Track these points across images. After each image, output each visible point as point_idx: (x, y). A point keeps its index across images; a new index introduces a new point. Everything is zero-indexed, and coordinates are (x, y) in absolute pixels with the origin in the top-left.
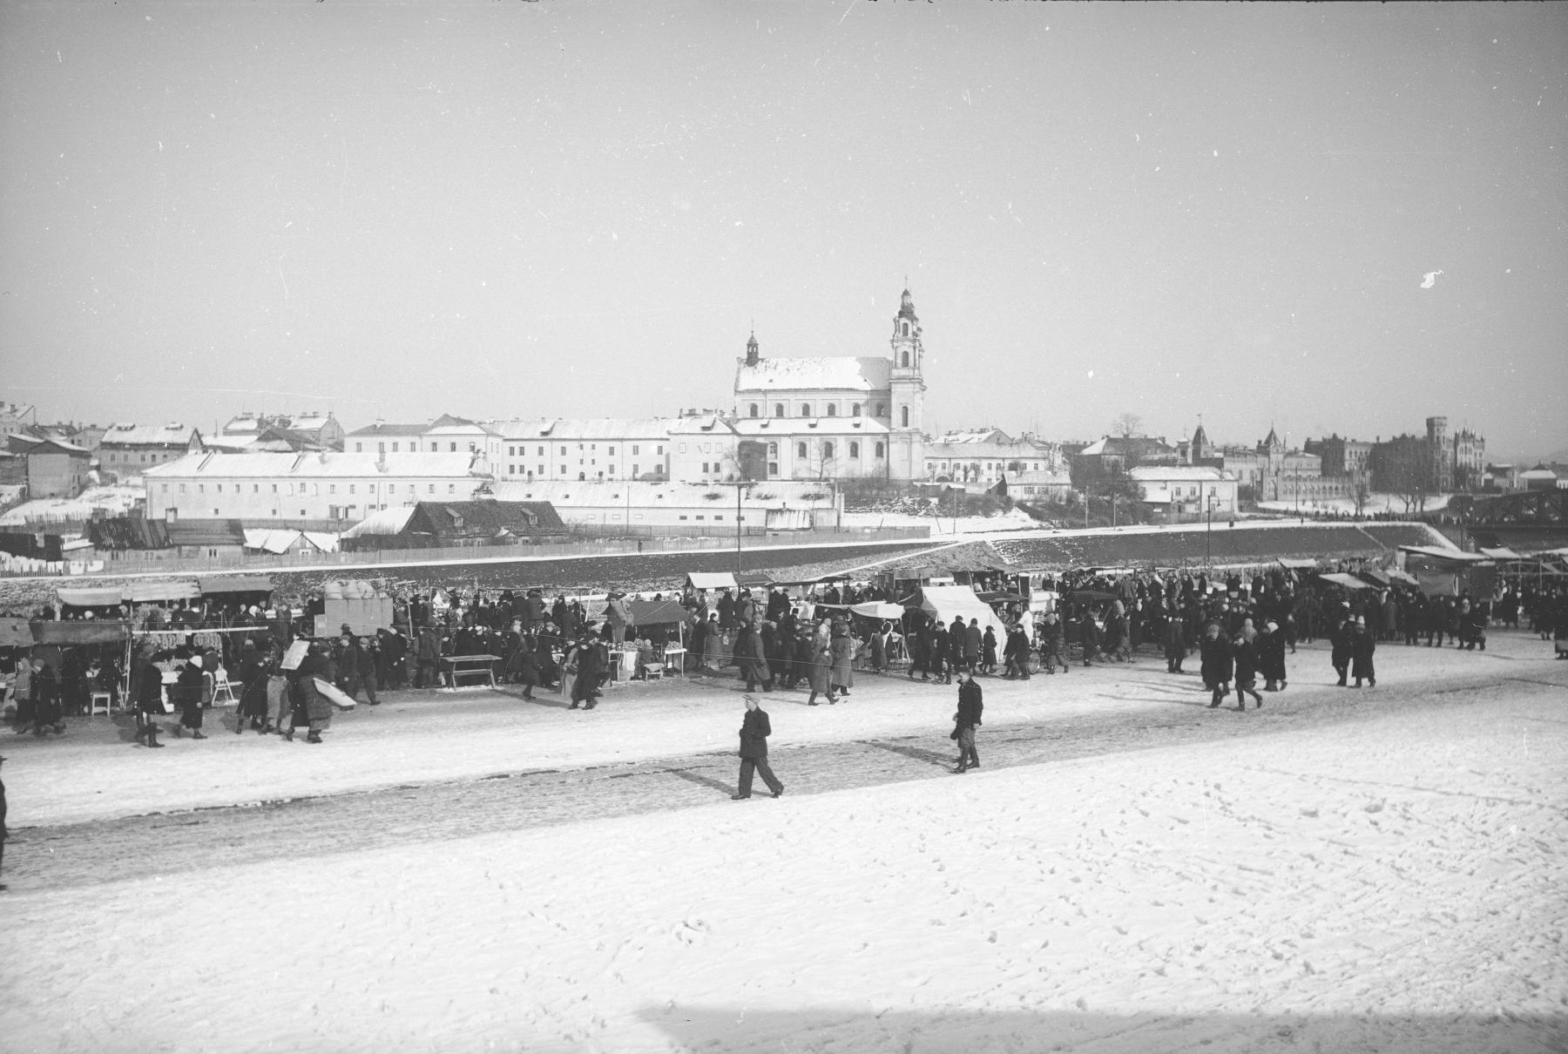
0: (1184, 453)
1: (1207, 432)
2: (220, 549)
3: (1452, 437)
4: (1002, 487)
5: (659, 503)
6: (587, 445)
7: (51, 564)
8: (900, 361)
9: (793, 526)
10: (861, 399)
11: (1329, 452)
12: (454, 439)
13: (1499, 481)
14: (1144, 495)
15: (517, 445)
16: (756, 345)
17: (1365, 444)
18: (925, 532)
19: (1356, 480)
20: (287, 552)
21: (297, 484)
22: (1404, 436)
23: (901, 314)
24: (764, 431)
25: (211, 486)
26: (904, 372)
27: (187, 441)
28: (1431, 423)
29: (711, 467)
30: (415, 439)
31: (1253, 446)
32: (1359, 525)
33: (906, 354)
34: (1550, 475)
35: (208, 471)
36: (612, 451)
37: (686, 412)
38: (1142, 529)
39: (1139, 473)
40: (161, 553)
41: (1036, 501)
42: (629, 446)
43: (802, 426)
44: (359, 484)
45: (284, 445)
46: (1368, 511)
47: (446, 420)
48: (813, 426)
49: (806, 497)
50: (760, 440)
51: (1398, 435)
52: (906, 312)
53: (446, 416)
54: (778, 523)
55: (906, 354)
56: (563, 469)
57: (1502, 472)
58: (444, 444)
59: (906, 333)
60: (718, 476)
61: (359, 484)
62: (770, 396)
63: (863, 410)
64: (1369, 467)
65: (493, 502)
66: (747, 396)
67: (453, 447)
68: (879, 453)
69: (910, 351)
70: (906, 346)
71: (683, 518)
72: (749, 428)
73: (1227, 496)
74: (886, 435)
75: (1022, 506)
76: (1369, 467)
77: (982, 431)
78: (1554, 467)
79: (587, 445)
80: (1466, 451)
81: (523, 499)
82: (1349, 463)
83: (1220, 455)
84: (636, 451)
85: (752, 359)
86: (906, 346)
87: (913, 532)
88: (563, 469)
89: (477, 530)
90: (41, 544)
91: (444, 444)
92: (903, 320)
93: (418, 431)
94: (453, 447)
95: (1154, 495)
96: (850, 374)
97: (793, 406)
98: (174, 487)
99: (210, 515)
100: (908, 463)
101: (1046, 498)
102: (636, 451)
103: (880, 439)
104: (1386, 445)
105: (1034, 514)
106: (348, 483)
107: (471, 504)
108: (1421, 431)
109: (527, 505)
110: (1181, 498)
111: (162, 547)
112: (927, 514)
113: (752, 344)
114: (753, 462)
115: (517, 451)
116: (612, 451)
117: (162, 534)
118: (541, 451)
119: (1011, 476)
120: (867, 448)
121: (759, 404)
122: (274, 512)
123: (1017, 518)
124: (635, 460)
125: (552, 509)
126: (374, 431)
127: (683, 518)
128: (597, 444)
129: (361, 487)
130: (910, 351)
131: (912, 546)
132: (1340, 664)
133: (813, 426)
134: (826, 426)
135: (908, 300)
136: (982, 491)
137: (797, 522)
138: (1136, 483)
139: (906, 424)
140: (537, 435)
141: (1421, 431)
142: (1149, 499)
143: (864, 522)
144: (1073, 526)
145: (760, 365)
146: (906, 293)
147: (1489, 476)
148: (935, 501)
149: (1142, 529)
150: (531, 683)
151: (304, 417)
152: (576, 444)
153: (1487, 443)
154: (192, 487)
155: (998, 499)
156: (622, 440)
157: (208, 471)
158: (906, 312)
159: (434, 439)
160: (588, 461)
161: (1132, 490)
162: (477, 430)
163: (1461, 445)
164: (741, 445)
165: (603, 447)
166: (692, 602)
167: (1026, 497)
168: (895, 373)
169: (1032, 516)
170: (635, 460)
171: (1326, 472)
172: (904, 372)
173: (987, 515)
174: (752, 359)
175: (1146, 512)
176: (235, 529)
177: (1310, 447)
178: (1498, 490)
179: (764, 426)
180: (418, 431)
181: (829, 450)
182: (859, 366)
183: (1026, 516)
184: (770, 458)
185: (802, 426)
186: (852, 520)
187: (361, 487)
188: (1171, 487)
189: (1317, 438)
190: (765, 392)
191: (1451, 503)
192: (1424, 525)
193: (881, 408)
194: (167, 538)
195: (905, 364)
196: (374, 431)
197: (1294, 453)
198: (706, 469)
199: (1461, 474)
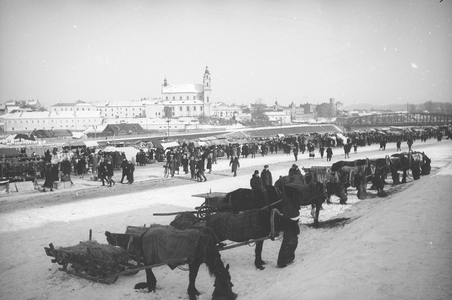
0: (275, 108)
1: (294, 102)
2: (67, 137)
3: (335, 103)
4: (234, 118)
5: (154, 123)
7: (34, 142)
8: (206, 85)
9: (192, 129)
10: (195, 95)
11: (306, 107)
12: (83, 107)
13: (346, 114)
14: (269, 119)
15: (99, 109)
17: (315, 105)
18: (225, 129)
19: (314, 114)
20: (81, 138)
21: (50, 120)
22: (324, 103)
23: (206, 73)
24: (170, 104)
25: (24, 121)
26: (207, 88)
27: (4, 108)
28: (331, 100)
29: (158, 114)
30: (72, 107)
31: (288, 106)
32: (320, 125)
33: (208, 83)
34: (357, 112)
35: (23, 117)
36: (126, 110)
37: (143, 98)
38: (270, 128)
39: (267, 113)
40: (53, 138)
41: (243, 121)
42: (131, 108)
43: (180, 102)
44: (69, 120)
45: (30, 109)
46: (319, 122)
47: (79, 102)
48: (183, 102)
49: (192, 121)
50: (170, 106)
51: (323, 103)
52: (207, 72)
54: (188, 128)
55: (208, 83)
56: (112, 115)
57: (346, 112)
58: (80, 109)
59: (207, 78)
60: (160, 116)
61: (68, 120)
62: (171, 95)
63: (196, 98)
64: (316, 111)
65: (125, 124)
66: (165, 95)
67: (83, 109)
68: (201, 109)
69: (209, 82)
70: (207, 81)
71: (161, 127)
72: (167, 103)
73: (287, 119)
74: (203, 105)
75: (240, 122)
76: (316, 111)
77: (218, 103)
78: (358, 110)
79: (119, 108)
80: (339, 107)
81: (115, 123)
82: (311, 110)
83: (282, 108)
84: (133, 109)
85: (165, 85)
86: (207, 81)
87: (222, 129)
88: (112, 115)
89: (123, 131)
90: (29, 137)
91: (80, 109)
92: (207, 74)
93: (73, 105)
94: (83, 109)
95: (271, 119)
96: (192, 88)
97: (177, 97)
98: (12, 122)
99: (25, 129)
100: (209, 112)
101: (246, 120)
102: (133, 109)
103: (201, 106)
104: (321, 105)
105: (243, 124)
106: (66, 120)
107: (120, 124)
108: (328, 102)
109: (117, 125)
110: (277, 120)
111: (53, 137)
112: (216, 125)
113: (165, 80)
114: (168, 112)
116: (126, 110)
117: (52, 133)
118: (106, 110)
119: (236, 115)
120: (198, 108)
122: (26, 128)
123: (239, 125)
124: (133, 112)
125: (140, 125)
126: (59, 105)
127: (161, 127)
128: (122, 108)
129: (70, 121)
130: (209, 82)
131: (224, 133)
132: (381, 147)
133: (183, 102)
134: (187, 102)
135: (207, 69)
136: (228, 119)
137: (193, 127)
138: (267, 116)
140: (105, 106)
141: (328, 102)
142: (270, 120)
143: (207, 127)
144: (253, 127)
145: (168, 86)
146: (207, 67)
147: (344, 113)
148: (218, 122)
149: (270, 128)
150: (170, 167)
151: (29, 101)
152: (116, 108)
153: (344, 105)
154: (18, 122)
155: (233, 121)
156: (129, 107)
157: (23, 117)
158: (207, 72)
159: (78, 107)
160: (119, 113)
161: (267, 118)
162: (89, 105)
163: (338, 105)
164: (165, 107)
165: (124, 109)
167: (240, 120)
168: (205, 88)
169: (243, 125)
170: (133, 112)
171: (305, 112)
172: (207, 88)
173: (231, 125)
174: (165, 85)
175: (270, 123)
176: (69, 132)
177: (301, 106)
178: (346, 116)
180: (73, 105)
181: (188, 109)
182: (194, 86)
183: (241, 125)
184: (173, 111)
185: (180, 102)
186: (200, 127)
187: (70, 121)
188: (275, 117)
189: (303, 104)
190: (170, 93)
191: (337, 120)
192: (334, 125)
193: (201, 96)
194: (54, 135)
195: (208, 86)
196: (59, 105)
197: (297, 108)
198: (156, 114)
199: (338, 113)
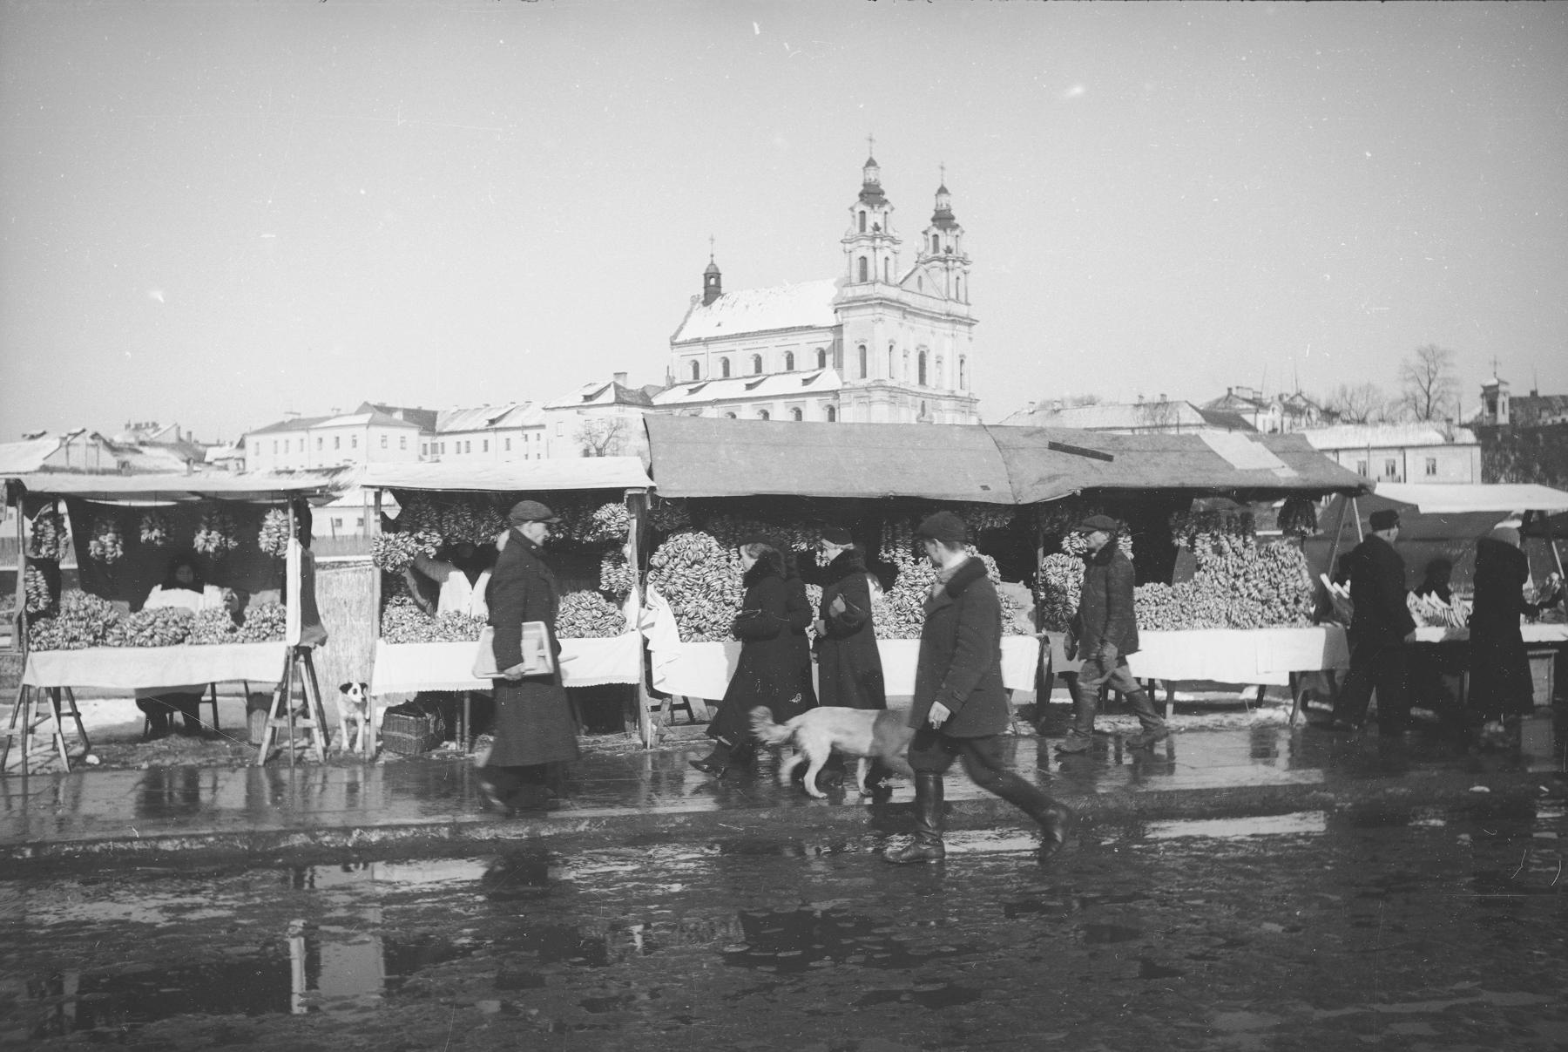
6: (532, 434)
16: (718, 276)
30: (303, 434)
53: (366, 404)
62: (713, 347)
66: (686, 350)
115: (463, 446)
121: (701, 360)
139: (864, 375)
140: (579, 400)
159: (336, 515)
166: (649, 874)
174: (712, 290)
179: (749, 387)
185: (793, 384)
190: (706, 342)
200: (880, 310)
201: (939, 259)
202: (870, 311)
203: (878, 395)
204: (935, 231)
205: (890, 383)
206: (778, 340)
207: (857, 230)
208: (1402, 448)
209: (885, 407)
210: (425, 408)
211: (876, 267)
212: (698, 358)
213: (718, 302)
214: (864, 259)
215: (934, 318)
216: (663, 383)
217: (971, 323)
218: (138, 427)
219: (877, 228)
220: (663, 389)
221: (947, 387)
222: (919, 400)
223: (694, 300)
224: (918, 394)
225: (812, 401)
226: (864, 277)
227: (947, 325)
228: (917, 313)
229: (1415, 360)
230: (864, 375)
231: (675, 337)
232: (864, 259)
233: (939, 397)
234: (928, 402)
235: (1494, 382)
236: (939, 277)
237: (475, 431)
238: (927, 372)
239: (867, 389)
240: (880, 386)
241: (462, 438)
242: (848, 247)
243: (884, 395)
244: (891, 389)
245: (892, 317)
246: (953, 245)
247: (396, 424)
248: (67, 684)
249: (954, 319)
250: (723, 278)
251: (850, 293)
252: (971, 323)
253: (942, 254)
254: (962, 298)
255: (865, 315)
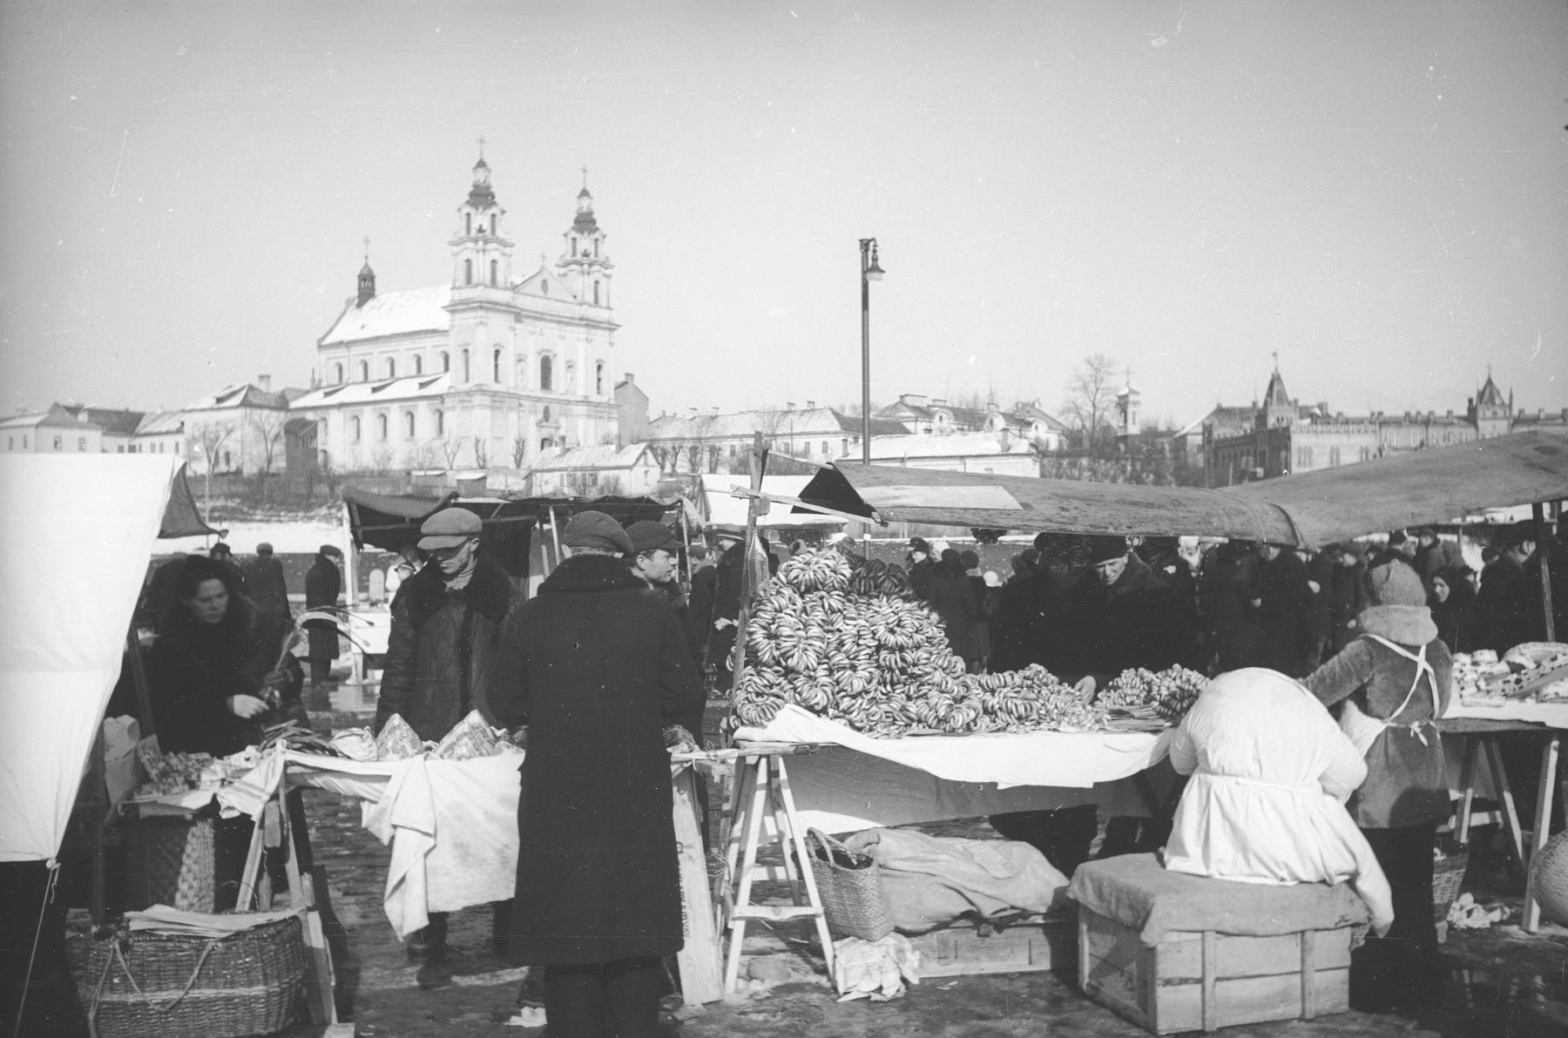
16: (372, 278)
53: (56, 405)
62: (354, 350)
66: (332, 353)
139: (467, 380)
174: (367, 288)
200: (481, 313)
201: (576, 263)
202: (472, 314)
203: (478, 399)
204: (573, 234)
205: (495, 387)
206: (408, 343)
207: (464, 232)
208: (962, 457)
209: (488, 413)
210: (132, 409)
211: (481, 271)
212: (366, 358)
213: (370, 303)
214: (468, 261)
215: (561, 321)
216: (307, 386)
217: (611, 327)
218: (132, 449)
219: (480, 230)
220: (308, 392)
221: (580, 393)
222: (541, 406)
223: (349, 302)
224: (539, 400)
225: (422, 404)
226: (469, 281)
227: (582, 330)
228: (538, 317)
229: (1087, 371)
230: (467, 380)
231: (323, 338)
232: (494, 262)
233: (568, 402)
234: (554, 408)
235: (1125, 391)
236: (581, 283)
237: (167, 433)
238: (554, 377)
239: (468, 393)
240: (482, 391)
241: (156, 440)
242: (455, 249)
243: (487, 400)
244: (494, 394)
245: (500, 322)
246: (591, 249)
247: (81, 426)
248: (407, 761)
249: (591, 324)
250: (377, 280)
251: (467, 294)
252: (611, 327)
253: (579, 257)
254: (603, 301)
255: (470, 318)
